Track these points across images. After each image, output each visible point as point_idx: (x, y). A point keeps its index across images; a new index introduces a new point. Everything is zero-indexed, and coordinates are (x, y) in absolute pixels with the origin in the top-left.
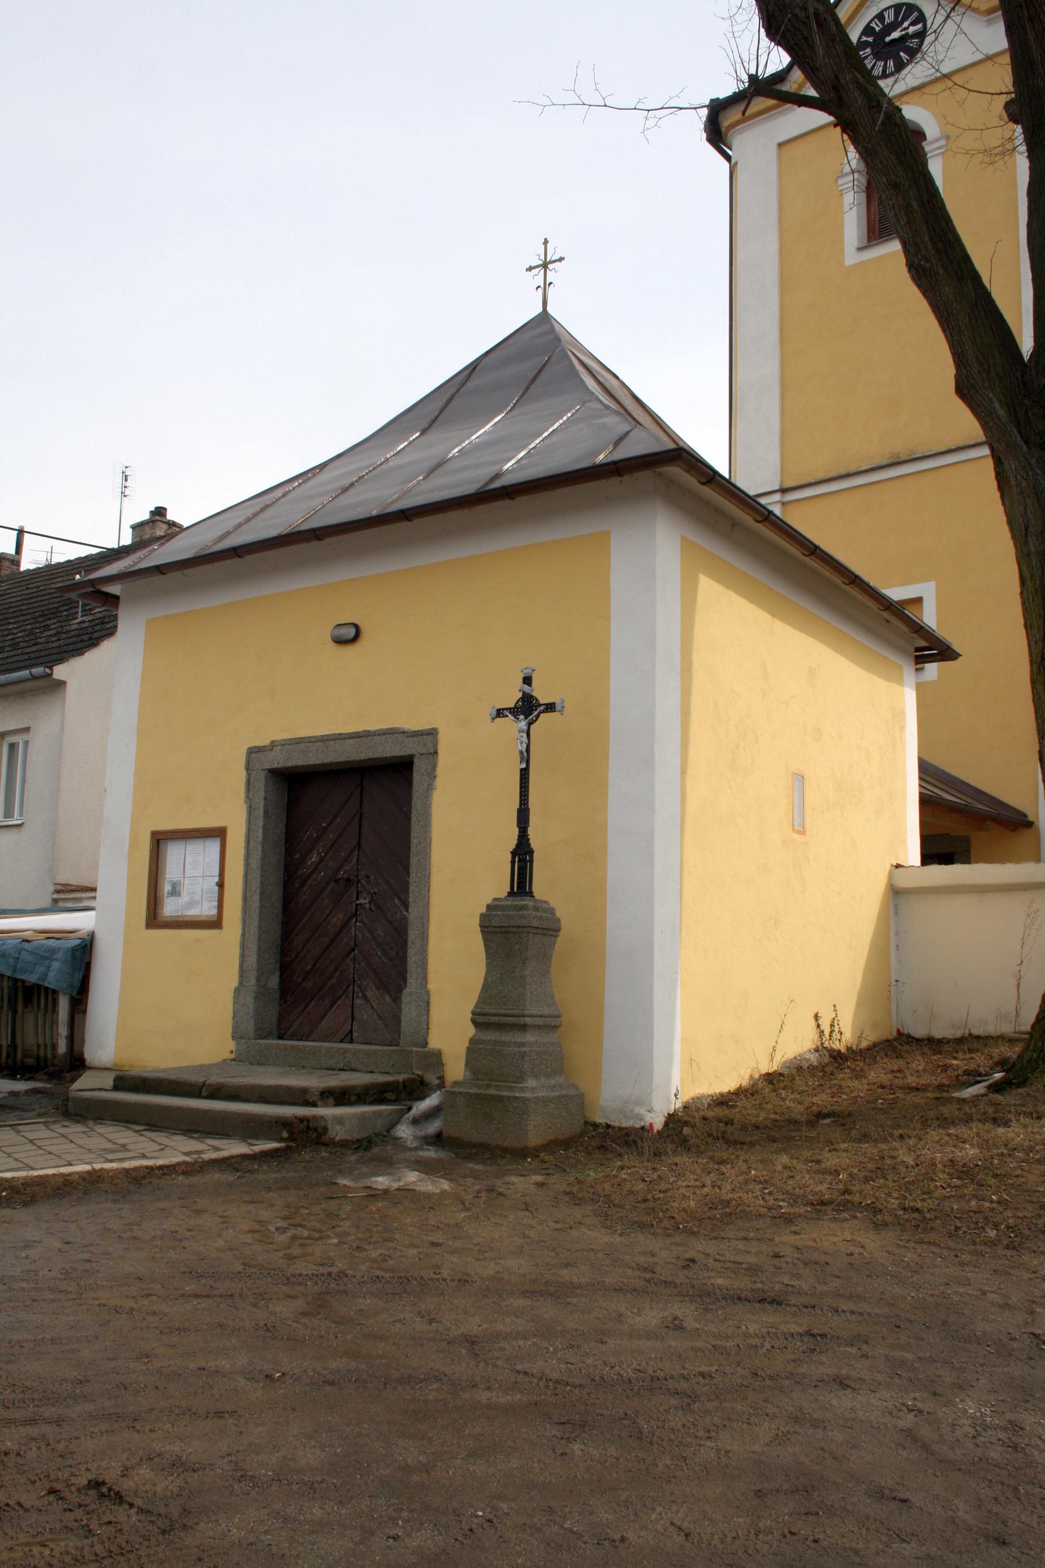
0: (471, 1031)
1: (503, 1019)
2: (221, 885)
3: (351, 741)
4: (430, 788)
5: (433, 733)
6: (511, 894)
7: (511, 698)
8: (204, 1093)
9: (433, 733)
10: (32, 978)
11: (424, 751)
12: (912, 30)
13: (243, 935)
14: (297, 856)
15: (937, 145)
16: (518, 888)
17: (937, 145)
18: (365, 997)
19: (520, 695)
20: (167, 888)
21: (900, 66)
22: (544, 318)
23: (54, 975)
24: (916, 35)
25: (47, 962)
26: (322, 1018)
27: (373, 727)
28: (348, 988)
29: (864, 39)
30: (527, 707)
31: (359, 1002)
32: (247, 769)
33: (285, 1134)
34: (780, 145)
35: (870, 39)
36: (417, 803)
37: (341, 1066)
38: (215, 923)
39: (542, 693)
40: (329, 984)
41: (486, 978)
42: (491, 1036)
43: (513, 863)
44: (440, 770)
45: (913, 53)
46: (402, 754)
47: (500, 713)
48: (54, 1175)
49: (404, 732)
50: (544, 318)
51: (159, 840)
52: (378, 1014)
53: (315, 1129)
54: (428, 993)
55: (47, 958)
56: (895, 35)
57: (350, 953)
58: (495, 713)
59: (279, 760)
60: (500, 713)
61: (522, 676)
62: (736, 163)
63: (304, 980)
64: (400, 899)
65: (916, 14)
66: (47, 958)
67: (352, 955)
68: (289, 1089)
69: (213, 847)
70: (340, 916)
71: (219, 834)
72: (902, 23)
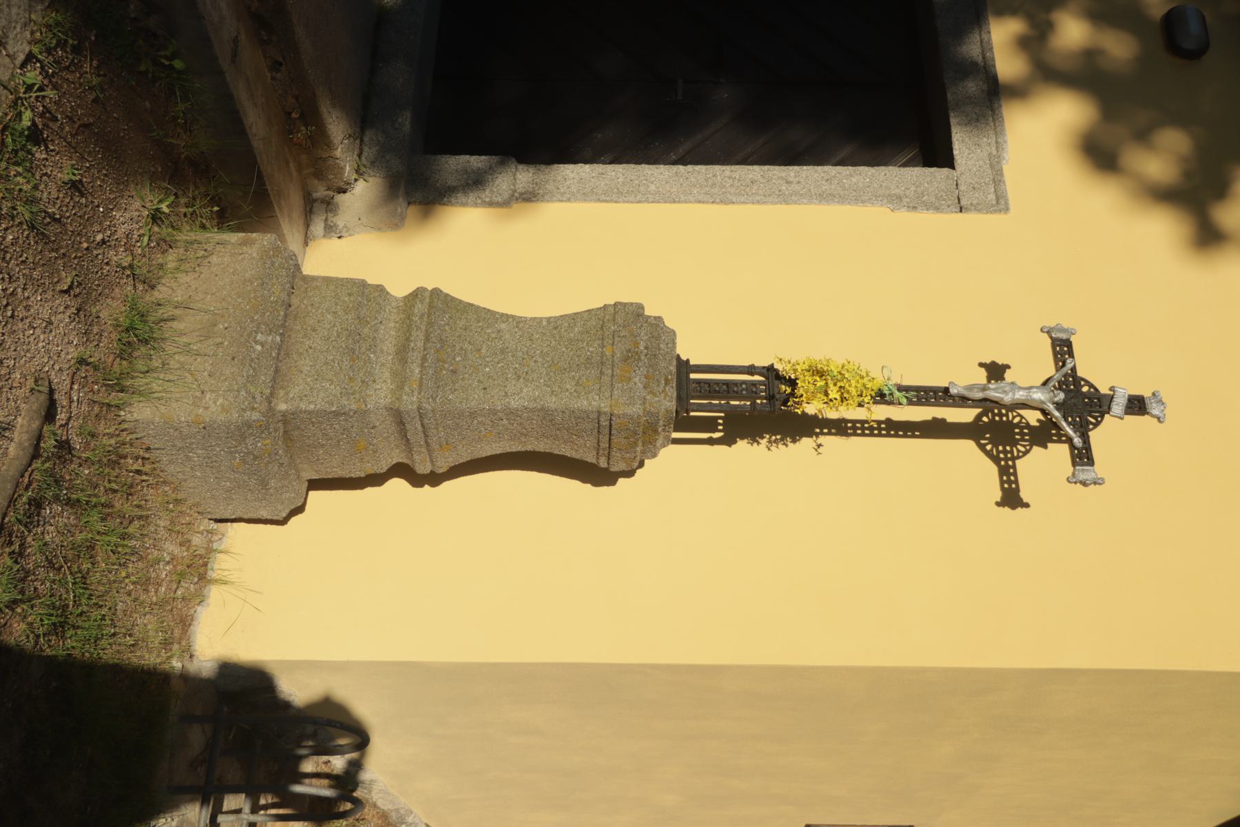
0: (430, 288)
4: (896, 201)
5: (1000, 204)
6: (684, 367)
7: (1094, 369)
9: (1000, 204)
11: (962, 188)
14: (147, 104)
16: (698, 382)
19: (1104, 390)
39: (1109, 436)
41: (506, 317)
43: (751, 370)
61: (1147, 394)
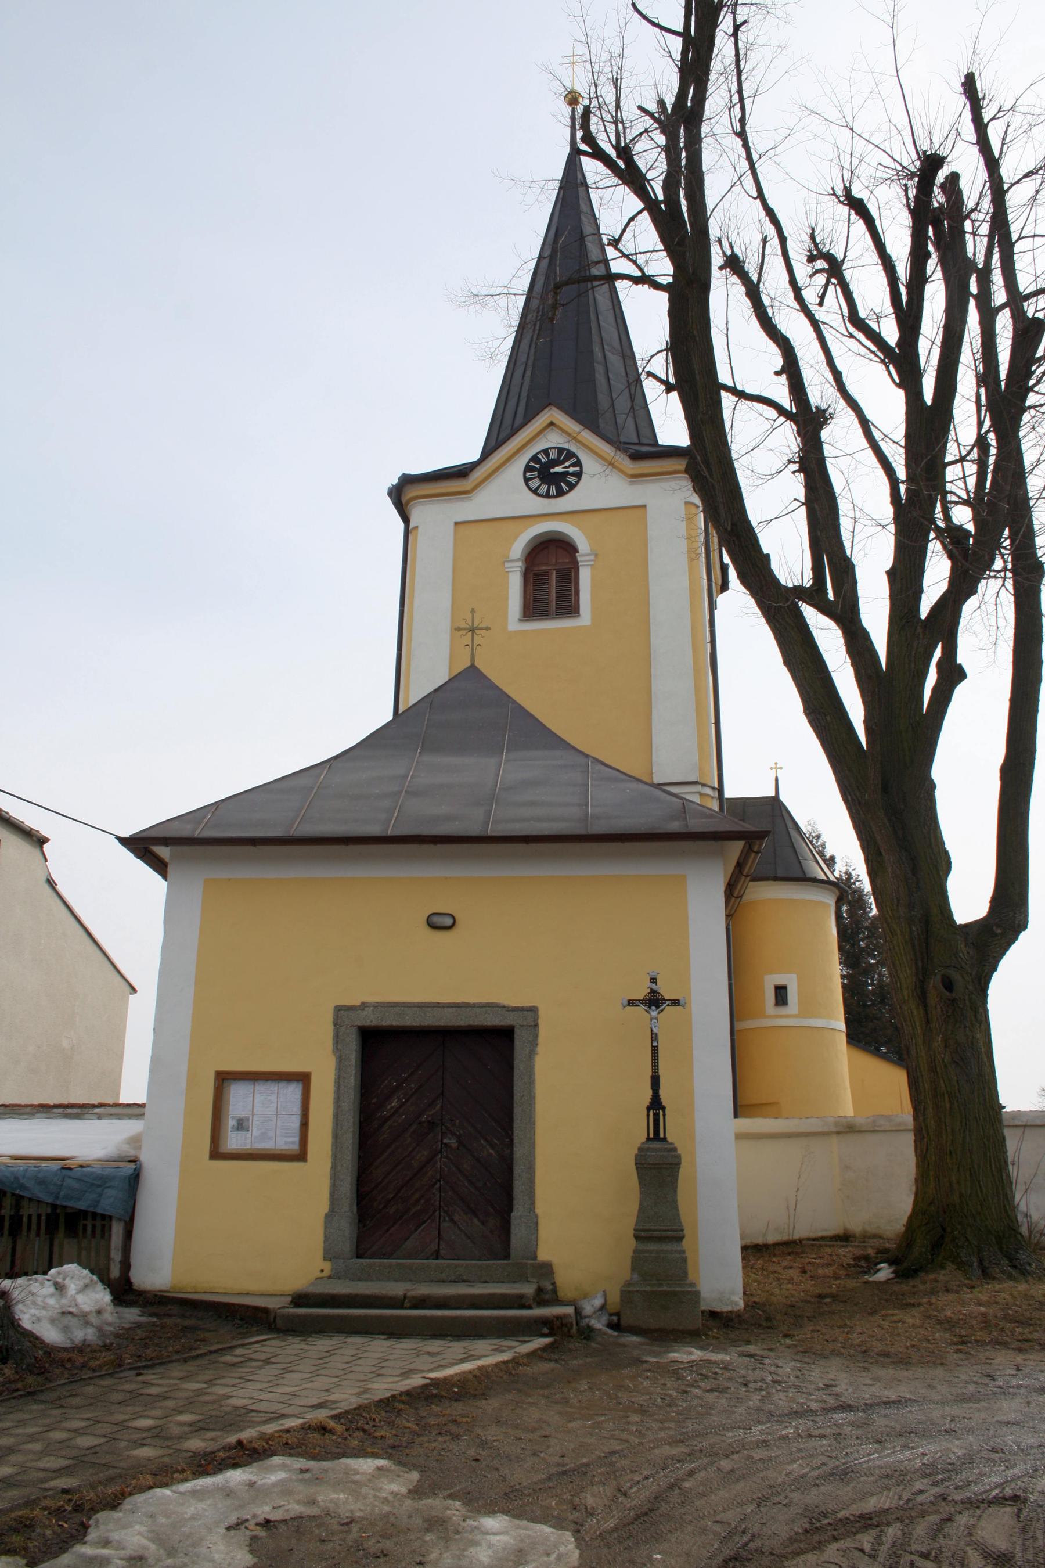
1: (664, 1234)
2: (304, 1125)
3: (450, 1010)
4: (532, 1053)
5: (534, 1010)
6: (648, 1139)
7: (641, 992)
8: (407, 1304)
9: (534, 1010)
10: (82, 1205)
12: (571, 470)
13: (334, 1167)
14: (374, 1101)
15: (587, 558)
17: (587, 558)
18: (452, 1220)
20: (232, 1123)
21: (560, 493)
22: (472, 672)
23: (109, 1202)
24: (573, 474)
25: (99, 1190)
26: (406, 1240)
27: (472, 1000)
28: (434, 1212)
29: (532, 464)
30: (654, 1001)
31: (445, 1225)
32: (335, 1025)
33: (546, 1331)
34: (456, 523)
35: (537, 466)
36: (519, 1065)
37: (453, 1278)
38: (300, 1156)
39: (666, 991)
40: (414, 1210)
42: (652, 1247)
44: (540, 1040)
45: (572, 487)
46: (502, 1024)
47: (631, 1003)
48: (497, 1365)
49: (504, 1007)
50: (472, 672)
51: (224, 1079)
52: (466, 1234)
53: (566, 1325)
54: (536, 1216)
55: (99, 1186)
56: (558, 469)
57: (435, 1183)
58: (626, 1003)
59: (370, 1019)
60: (631, 1003)
62: (416, 528)
63: (385, 1207)
64: (486, 1140)
65: (574, 460)
66: (99, 1186)
67: (438, 1186)
68: (504, 1296)
69: (293, 1092)
70: (425, 1153)
71: (304, 1079)
72: (563, 462)
